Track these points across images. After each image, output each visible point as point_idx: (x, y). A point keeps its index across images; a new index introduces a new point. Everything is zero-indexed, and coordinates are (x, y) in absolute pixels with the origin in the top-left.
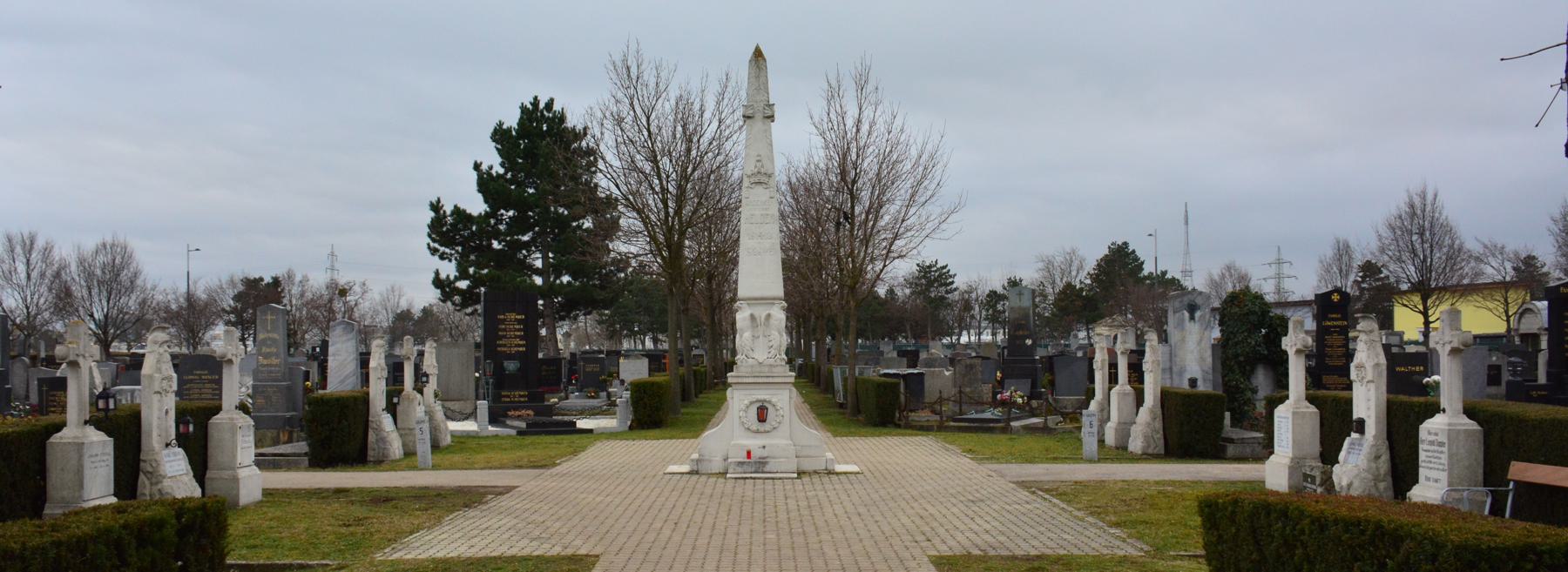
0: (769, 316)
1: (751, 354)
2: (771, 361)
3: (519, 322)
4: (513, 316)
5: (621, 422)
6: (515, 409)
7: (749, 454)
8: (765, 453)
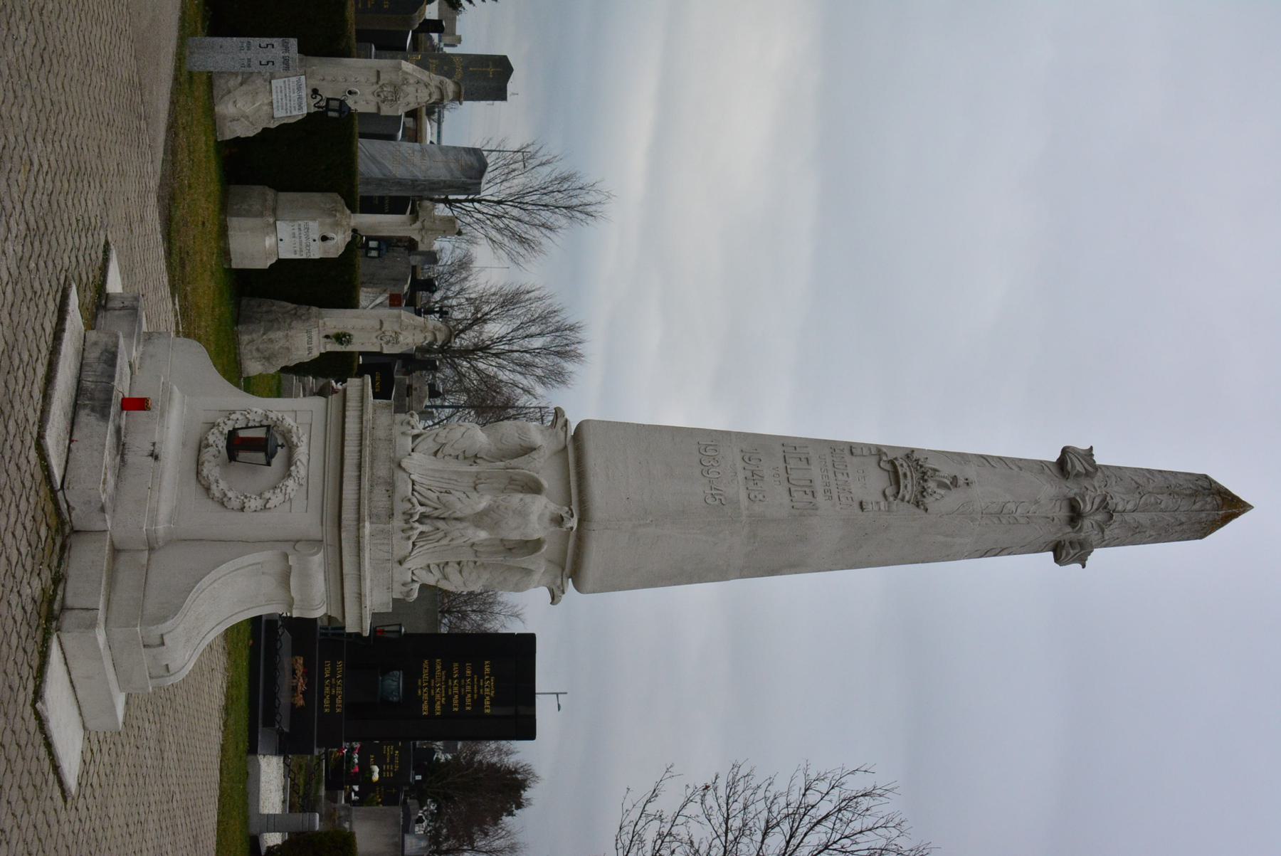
0: (534, 487)
1: (427, 444)
2: (404, 488)
3: (478, 702)
4: (489, 692)
5: (272, 823)
6: (308, 673)
7: (139, 404)
8: (137, 456)
